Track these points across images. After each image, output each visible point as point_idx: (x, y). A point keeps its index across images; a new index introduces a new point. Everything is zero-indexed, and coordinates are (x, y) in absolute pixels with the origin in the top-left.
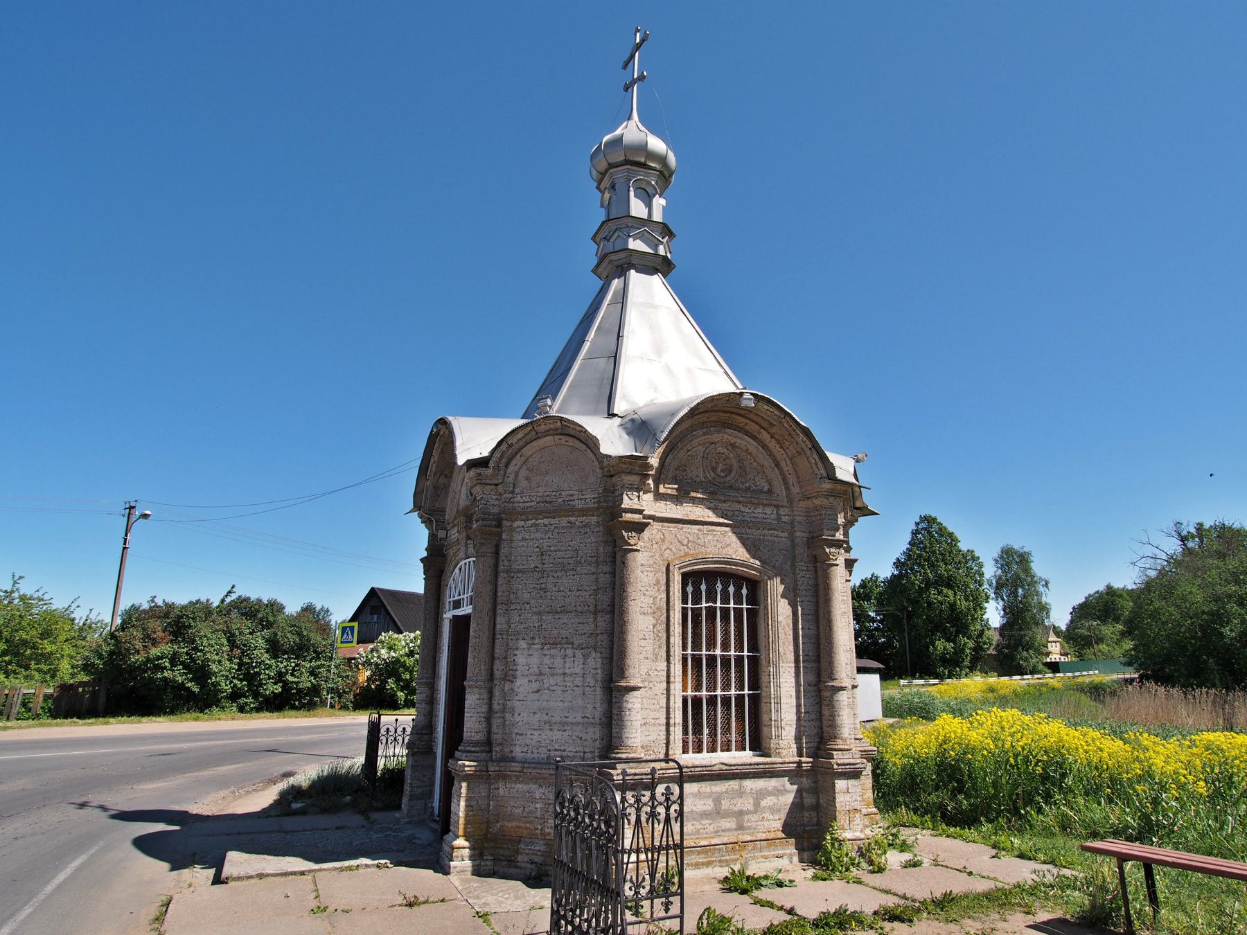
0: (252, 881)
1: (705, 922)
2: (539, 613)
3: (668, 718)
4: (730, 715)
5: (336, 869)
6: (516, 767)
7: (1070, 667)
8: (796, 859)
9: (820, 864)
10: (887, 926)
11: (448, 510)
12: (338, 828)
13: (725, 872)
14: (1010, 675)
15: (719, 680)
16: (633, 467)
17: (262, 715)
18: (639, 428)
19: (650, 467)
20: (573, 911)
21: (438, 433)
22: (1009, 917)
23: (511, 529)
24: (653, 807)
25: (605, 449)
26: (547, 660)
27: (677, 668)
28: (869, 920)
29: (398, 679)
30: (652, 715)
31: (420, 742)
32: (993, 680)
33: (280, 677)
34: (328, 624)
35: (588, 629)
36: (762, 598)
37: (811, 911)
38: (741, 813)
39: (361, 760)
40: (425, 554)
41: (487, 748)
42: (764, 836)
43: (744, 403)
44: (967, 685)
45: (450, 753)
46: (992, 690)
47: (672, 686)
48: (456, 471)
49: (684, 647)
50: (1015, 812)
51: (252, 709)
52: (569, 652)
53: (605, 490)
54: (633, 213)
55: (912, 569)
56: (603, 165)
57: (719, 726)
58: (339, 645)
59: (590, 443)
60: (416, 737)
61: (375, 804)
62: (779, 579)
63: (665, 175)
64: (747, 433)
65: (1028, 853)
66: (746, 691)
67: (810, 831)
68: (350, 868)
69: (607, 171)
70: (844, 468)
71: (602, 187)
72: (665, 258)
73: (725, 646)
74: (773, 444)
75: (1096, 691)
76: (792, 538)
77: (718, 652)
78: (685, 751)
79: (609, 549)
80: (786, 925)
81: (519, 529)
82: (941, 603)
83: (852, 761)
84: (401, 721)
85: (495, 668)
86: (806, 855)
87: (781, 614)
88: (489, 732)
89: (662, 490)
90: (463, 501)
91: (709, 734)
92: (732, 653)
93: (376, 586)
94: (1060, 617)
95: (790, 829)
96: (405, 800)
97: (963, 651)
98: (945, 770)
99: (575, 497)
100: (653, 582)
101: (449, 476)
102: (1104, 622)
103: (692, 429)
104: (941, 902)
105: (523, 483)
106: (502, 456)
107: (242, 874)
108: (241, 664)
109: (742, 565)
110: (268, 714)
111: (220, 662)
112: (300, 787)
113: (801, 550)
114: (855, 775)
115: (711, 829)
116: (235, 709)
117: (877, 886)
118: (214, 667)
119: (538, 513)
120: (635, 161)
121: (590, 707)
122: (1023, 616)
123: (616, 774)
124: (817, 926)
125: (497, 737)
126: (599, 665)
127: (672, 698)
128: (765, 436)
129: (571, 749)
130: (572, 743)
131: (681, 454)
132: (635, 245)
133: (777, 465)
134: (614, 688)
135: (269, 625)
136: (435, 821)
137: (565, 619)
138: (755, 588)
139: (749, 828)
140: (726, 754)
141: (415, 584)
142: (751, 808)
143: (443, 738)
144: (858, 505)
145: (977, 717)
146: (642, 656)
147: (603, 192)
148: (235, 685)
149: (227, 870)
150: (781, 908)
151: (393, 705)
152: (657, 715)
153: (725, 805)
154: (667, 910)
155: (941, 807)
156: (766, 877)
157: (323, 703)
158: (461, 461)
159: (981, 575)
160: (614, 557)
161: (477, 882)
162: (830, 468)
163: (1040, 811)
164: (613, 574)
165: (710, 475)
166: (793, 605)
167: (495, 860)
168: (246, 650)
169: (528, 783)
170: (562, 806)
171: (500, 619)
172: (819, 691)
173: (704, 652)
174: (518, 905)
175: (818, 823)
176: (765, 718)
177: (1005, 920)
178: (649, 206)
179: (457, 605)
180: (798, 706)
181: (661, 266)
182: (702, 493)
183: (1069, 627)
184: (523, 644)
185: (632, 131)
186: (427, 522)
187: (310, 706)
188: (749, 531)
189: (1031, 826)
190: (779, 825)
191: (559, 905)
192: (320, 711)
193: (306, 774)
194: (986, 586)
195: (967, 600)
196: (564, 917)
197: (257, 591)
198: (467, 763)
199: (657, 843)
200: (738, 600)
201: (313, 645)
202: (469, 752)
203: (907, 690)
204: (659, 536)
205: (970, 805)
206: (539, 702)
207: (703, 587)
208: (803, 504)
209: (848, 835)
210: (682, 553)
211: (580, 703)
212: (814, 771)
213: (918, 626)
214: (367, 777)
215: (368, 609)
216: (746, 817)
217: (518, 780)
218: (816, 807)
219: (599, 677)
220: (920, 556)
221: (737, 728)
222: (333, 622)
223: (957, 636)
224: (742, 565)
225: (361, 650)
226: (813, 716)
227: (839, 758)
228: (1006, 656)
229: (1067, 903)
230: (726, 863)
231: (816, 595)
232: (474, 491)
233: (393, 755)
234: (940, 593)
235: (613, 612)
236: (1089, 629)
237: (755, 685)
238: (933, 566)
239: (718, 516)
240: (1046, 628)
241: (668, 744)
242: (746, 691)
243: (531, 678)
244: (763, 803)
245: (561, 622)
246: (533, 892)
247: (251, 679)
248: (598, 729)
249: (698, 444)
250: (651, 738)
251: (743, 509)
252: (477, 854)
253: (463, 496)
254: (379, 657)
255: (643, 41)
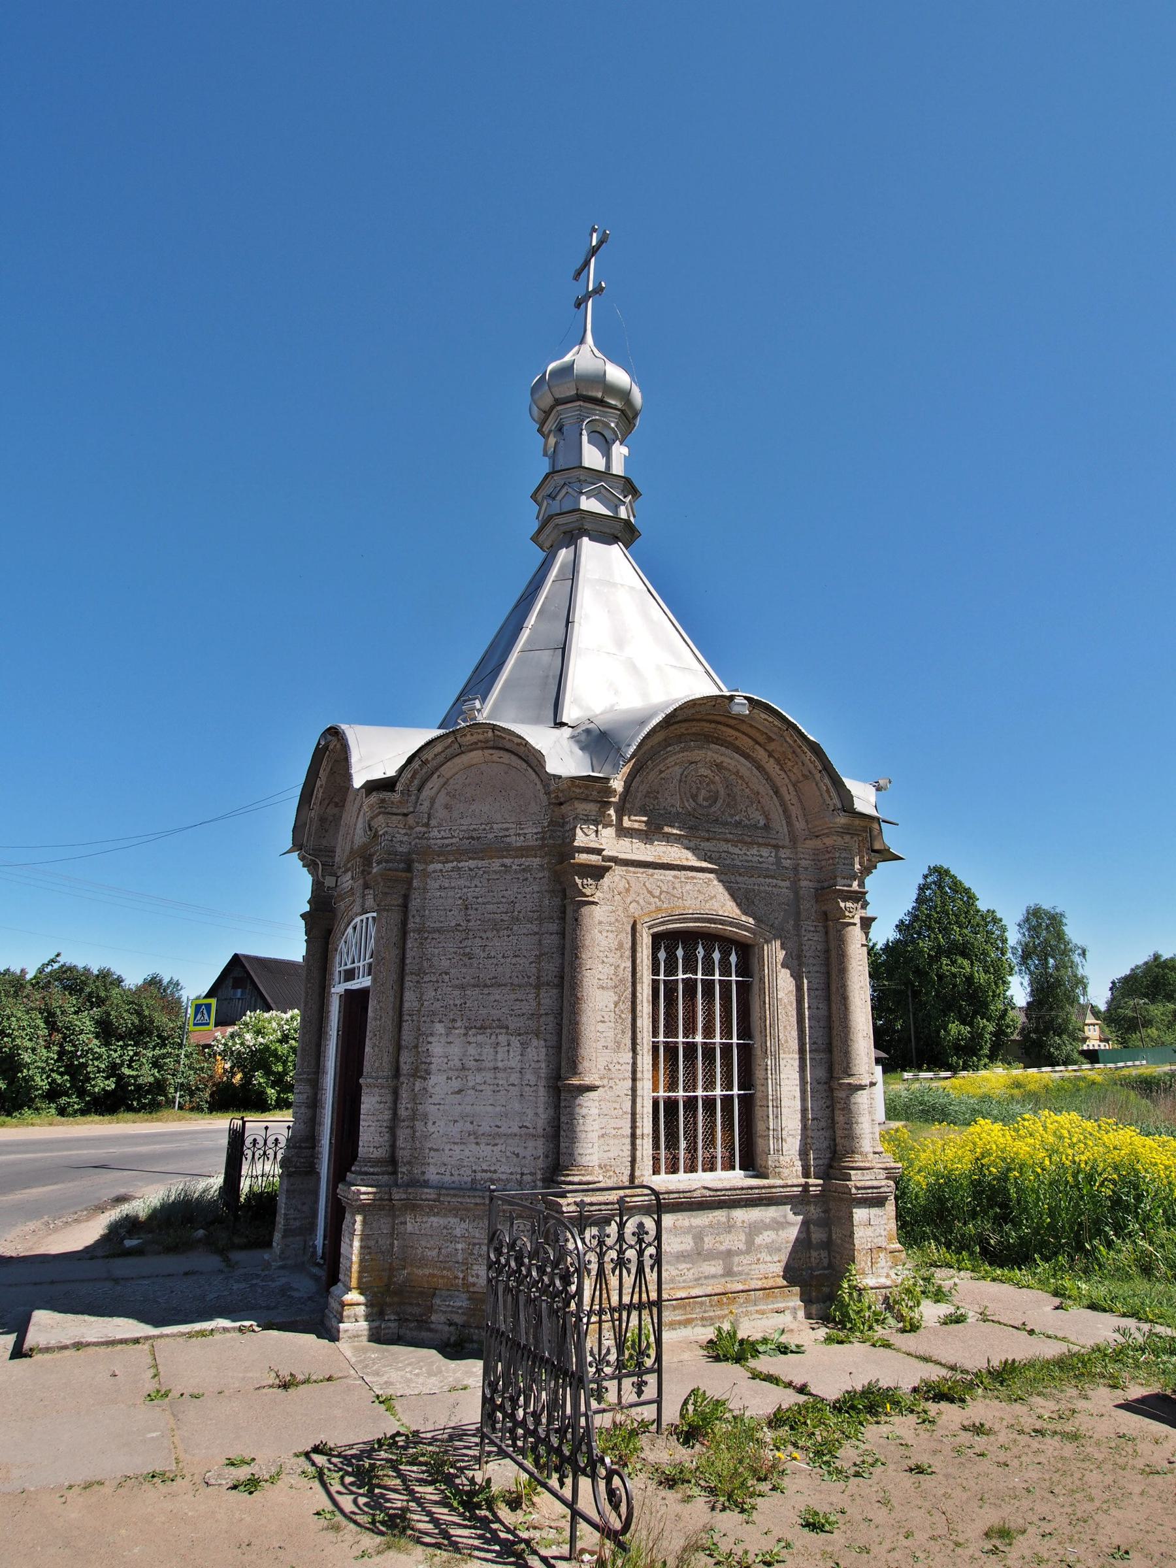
0: (67, 1353)
1: (691, 1408)
2: (462, 987)
3: (634, 1127)
4: (714, 1122)
5: (183, 1334)
6: (429, 1193)
7: (1112, 1057)
8: (801, 1314)
9: (834, 1320)
10: (932, 1407)
11: (338, 850)
12: (186, 1274)
13: (709, 1333)
14: (1039, 1066)
15: (700, 1077)
16: (589, 791)
17: (89, 1118)
18: (598, 741)
19: (613, 792)
20: (514, 1401)
21: (326, 747)
22: (1090, 1393)
23: (426, 874)
24: (621, 1252)
25: (552, 767)
26: (472, 1050)
27: (645, 1061)
28: (908, 1400)
29: (268, 1072)
30: (613, 1123)
31: (299, 1156)
32: (1018, 1072)
33: (113, 1070)
34: (178, 1001)
35: (526, 1008)
36: (756, 968)
37: (830, 1389)
38: (729, 1254)
39: (218, 1181)
40: (307, 908)
41: (390, 1169)
42: (759, 1284)
43: (736, 710)
44: (987, 1080)
45: (340, 1172)
46: (1018, 1085)
47: (639, 1084)
48: (350, 797)
49: (655, 1033)
50: (1080, 1248)
51: (76, 1112)
52: (503, 1039)
53: (551, 823)
54: (586, 464)
55: (919, 934)
56: (548, 401)
57: (700, 1137)
58: (191, 1028)
59: (532, 759)
60: (293, 1151)
61: (236, 1240)
62: (778, 943)
63: (628, 416)
64: (737, 750)
65: (1103, 1303)
66: (736, 1091)
67: (819, 1276)
68: (202, 1334)
69: (552, 408)
70: (865, 798)
71: (546, 429)
72: (627, 522)
73: (708, 1031)
74: (771, 766)
75: (1147, 1086)
76: (795, 888)
77: (699, 1039)
78: (656, 1171)
79: (557, 901)
80: (801, 1409)
81: (436, 878)
82: (954, 975)
83: (875, 1183)
84: (275, 1126)
85: (402, 1060)
86: (814, 1309)
87: (781, 986)
88: (393, 1146)
89: (626, 823)
90: (360, 837)
91: (686, 1149)
92: (717, 1040)
93: (240, 951)
94: (1098, 995)
95: (792, 1274)
96: (277, 1236)
97: (981, 1036)
98: (983, 1192)
99: (512, 832)
100: (614, 945)
101: (341, 805)
102: (1153, 1001)
103: (667, 743)
104: (999, 1374)
105: (441, 813)
106: (413, 777)
107: (53, 1343)
108: (61, 1054)
109: (731, 924)
110: (97, 1118)
111: (34, 1050)
112: (136, 1217)
113: (807, 905)
114: (878, 1202)
115: (690, 1275)
116: (53, 1111)
117: (912, 1350)
118: (26, 1057)
119: (461, 854)
120: (590, 395)
121: (530, 1112)
122: (1054, 994)
123: (568, 1205)
124: (840, 1410)
125: (403, 1154)
126: (542, 1057)
127: (639, 1100)
128: (761, 754)
129: (504, 1170)
130: (508, 1161)
131: (652, 775)
132: (589, 504)
133: (777, 793)
134: (562, 1088)
135: (101, 1002)
136: (318, 1264)
137: (497, 994)
138: (746, 955)
139: (740, 1273)
140: (709, 1175)
141: (292, 947)
142: (742, 1247)
143: (332, 1153)
144: (877, 846)
145: (1015, 1124)
146: (600, 1045)
147: (546, 437)
148: (54, 1080)
149: (33, 1338)
150: (789, 1385)
151: (261, 1105)
152: (620, 1123)
153: (709, 1242)
154: (640, 1393)
155: (982, 1241)
156: (765, 1341)
157: (170, 1103)
158: (358, 782)
159: (1004, 941)
160: (564, 912)
161: (376, 1352)
162: (846, 797)
163: (1109, 1245)
164: (562, 934)
165: (690, 805)
166: (797, 977)
167: (402, 1319)
168: (69, 1034)
169: (445, 1216)
170: (499, 1253)
171: (409, 996)
172: (831, 1090)
173: (681, 1039)
174: (432, 1384)
175: (830, 1266)
176: (760, 1126)
177: (1086, 1398)
178: (607, 455)
179: (350, 975)
180: (804, 1111)
181: (621, 533)
182: (679, 828)
183: (1110, 1004)
184: (439, 1028)
185: (585, 357)
186: (310, 865)
187: (153, 1108)
188: (740, 879)
189: (1100, 1265)
190: (779, 1269)
191: (494, 1390)
192: (165, 1113)
193: (148, 1198)
194: (1009, 955)
195: (986, 972)
196: (501, 1408)
197: (87, 957)
198: (363, 1189)
199: (635, 1314)
200: (725, 971)
201: (157, 1028)
202: (366, 1173)
203: (917, 1085)
204: (622, 884)
205: (1020, 1237)
206: (463, 1109)
207: (680, 953)
208: (810, 844)
209: (870, 1281)
210: (653, 907)
211: (517, 1106)
212: (824, 1196)
213: (938, 1002)
214: (226, 1204)
215: (230, 982)
216: (736, 1259)
217: (432, 1211)
218: (828, 1245)
219: (543, 1072)
220: (929, 916)
221: (723, 1140)
222: (184, 999)
223: (974, 1017)
224: (731, 924)
225: (218, 1034)
226: (823, 1124)
227: (858, 1179)
228: (1034, 1042)
229: (1164, 1372)
230: (710, 1321)
231: (827, 963)
232: (375, 824)
233: (261, 1173)
234: (954, 962)
235: (561, 986)
236: (1134, 1009)
237: (747, 1081)
238: (946, 931)
239: (699, 859)
240: (1083, 1008)
241: (633, 1161)
242: (736, 1091)
243: (451, 1074)
244: (758, 1240)
245: (492, 998)
246: (453, 1364)
247: (76, 1072)
248: (540, 1142)
249: (674, 763)
250: (611, 1155)
251: (732, 849)
252: (376, 1312)
253: (359, 831)
254: (242, 1044)
255: (601, 242)
